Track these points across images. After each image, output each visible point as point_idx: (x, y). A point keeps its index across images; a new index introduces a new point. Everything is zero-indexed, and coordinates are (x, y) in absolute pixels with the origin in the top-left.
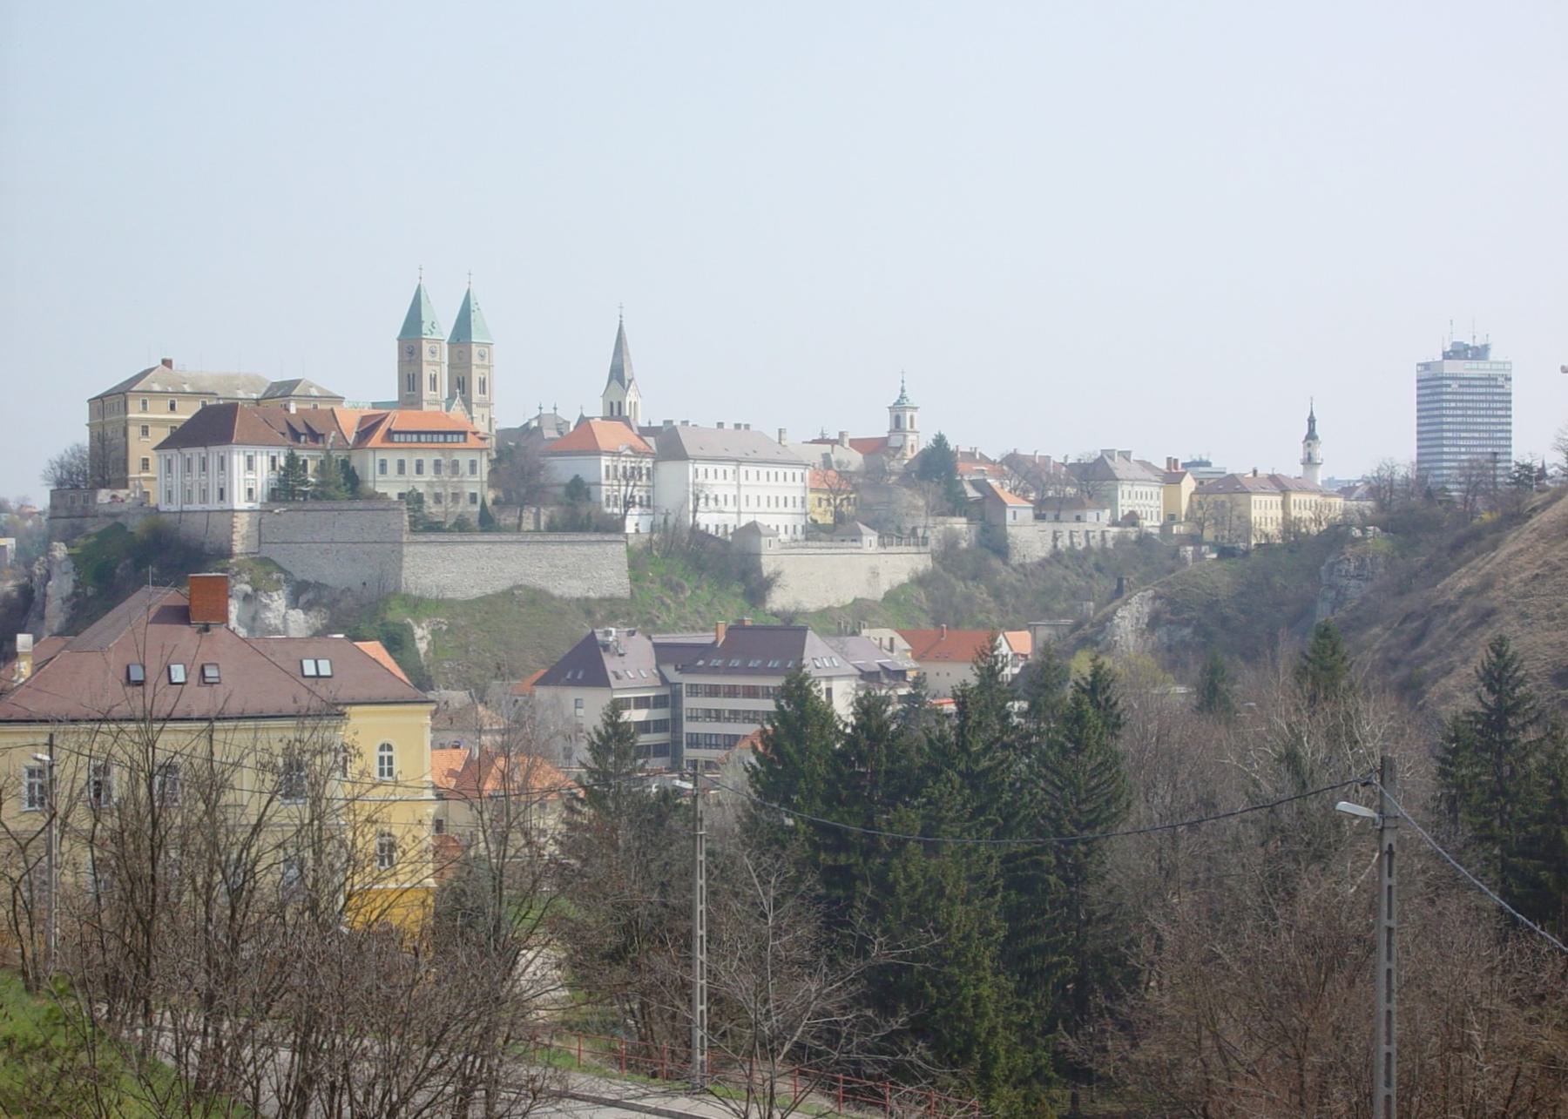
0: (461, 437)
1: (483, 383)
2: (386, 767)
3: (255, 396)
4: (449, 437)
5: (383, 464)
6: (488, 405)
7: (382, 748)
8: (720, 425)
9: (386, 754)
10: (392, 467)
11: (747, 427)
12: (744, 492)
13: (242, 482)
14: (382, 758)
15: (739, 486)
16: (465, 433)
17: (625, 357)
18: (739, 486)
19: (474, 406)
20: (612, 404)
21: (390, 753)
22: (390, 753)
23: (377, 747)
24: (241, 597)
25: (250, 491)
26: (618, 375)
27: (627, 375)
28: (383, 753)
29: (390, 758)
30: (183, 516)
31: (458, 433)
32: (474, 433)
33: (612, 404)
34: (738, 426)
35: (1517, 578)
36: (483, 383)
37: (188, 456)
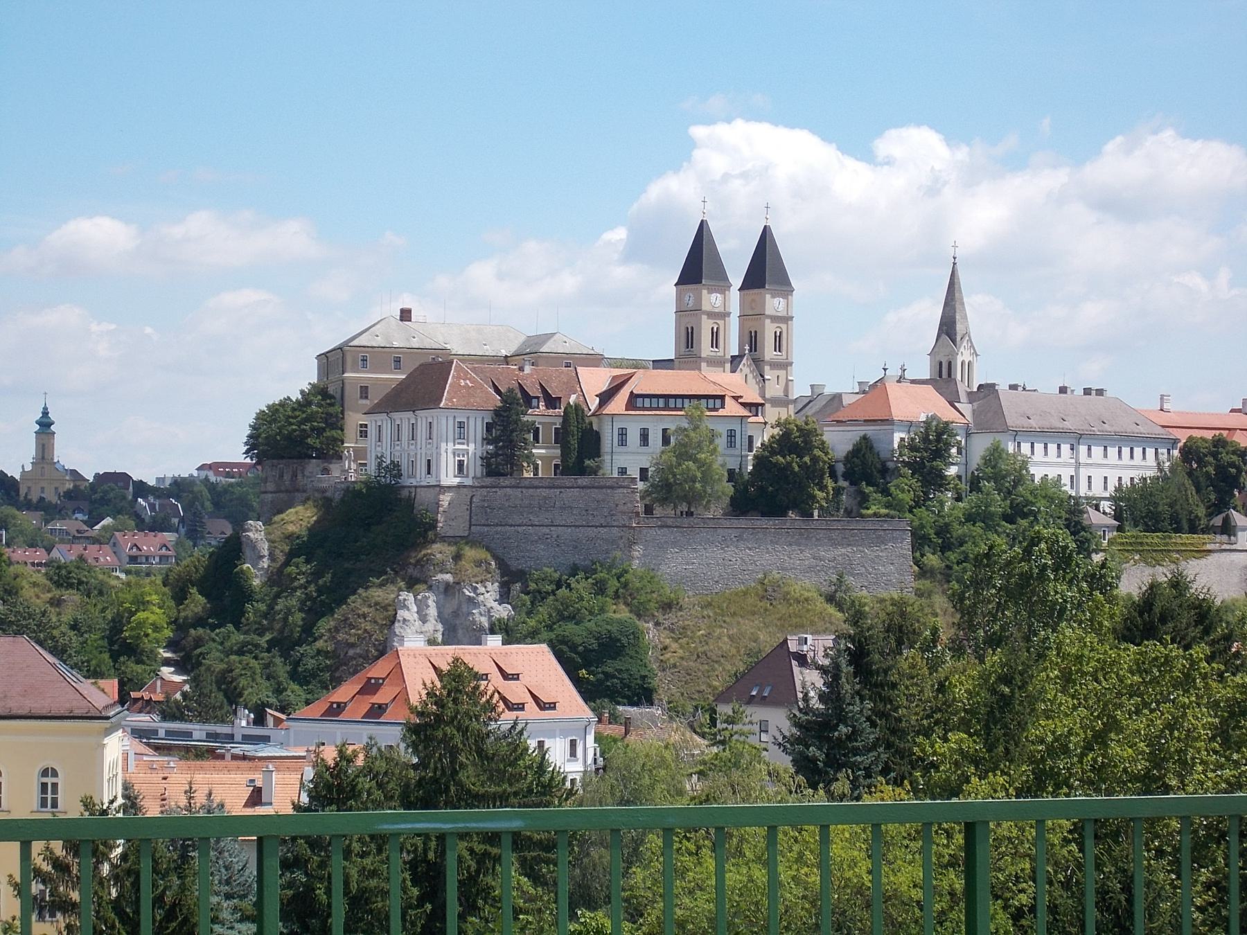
0: (718, 402)
1: (778, 339)
2: (49, 796)
3: (504, 353)
4: (672, 401)
5: (623, 433)
6: (785, 365)
7: (45, 773)
8: (1063, 390)
9: (49, 780)
10: (634, 437)
11: (1100, 392)
12: (1084, 473)
13: (450, 456)
14: (44, 786)
15: (1078, 465)
16: (722, 397)
17: (958, 306)
18: (1078, 465)
19: (767, 368)
20: (941, 364)
21: (54, 780)
22: (54, 780)
23: (37, 770)
24: (442, 589)
25: (461, 464)
26: (948, 328)
27: (959, 327)
28: (45, 780)
29: (55, 785)
30: (418, 490)
31: (715, 397)
32: (736, 398)
33: (941, 364)
34: (1087, 392)
35: (390, 613)
36: (778, 339)
37: (398, 422)
